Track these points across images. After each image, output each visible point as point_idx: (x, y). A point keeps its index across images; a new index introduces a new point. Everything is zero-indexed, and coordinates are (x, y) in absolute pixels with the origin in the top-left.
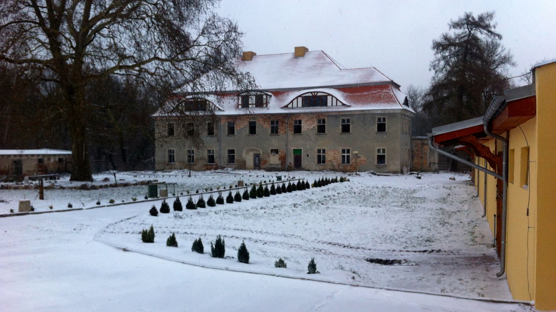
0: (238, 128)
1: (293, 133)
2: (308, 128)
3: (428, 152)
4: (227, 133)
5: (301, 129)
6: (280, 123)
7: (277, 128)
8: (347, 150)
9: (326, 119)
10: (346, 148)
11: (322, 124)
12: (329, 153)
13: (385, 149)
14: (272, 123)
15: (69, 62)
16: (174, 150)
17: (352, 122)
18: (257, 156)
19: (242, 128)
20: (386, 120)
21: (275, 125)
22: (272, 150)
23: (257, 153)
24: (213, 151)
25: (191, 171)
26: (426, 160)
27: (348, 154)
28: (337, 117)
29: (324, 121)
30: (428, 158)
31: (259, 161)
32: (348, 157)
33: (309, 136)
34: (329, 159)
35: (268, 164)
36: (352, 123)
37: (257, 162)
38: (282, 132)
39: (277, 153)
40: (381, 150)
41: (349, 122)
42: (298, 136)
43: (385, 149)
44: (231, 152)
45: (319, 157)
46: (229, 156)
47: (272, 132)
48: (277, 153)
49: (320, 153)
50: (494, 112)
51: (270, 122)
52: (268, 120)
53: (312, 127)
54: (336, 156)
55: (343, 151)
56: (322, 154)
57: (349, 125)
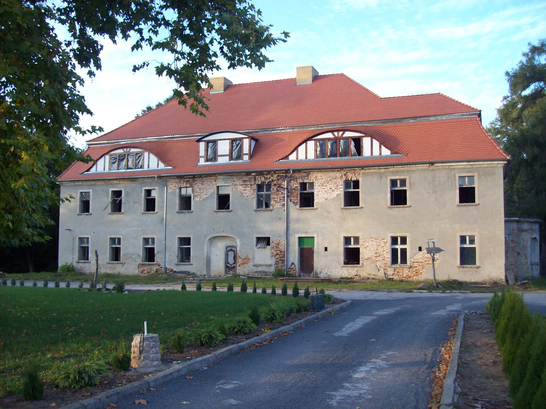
0: (197, 199)
1: (298, 206)
2: (326, 196)
3: (529, 243)
4: (177, 208)
5: (313, 200)
6: (274, 188)
7: (268, 197)
8: (470, 237)
9: (361, 180)
10: (399, 234)
11: (352, 190)
12: (367, 244)
13: (474, 237)
14: (260, 188)
15: (65, 102)
16: (88, 238)
17: (410, 184)
18: (231, 250)
19: (204, 199)
20: (476, 179)
21: (265, 192)
22: (259, 240)
23: (229, 243)
24: (153, 239)
25: (432, 278)
26: (526, 258)
27: (403, 247)
28: (381, 178)
29: (356, 184)
30: (529, 256)
31: (235, 258)
32: (404, 251)
33: (329, 212)
34: (366, 257)
35: (251, 264)
36: (410, 188)
37: (231, 261)
38: (278, 205)
39: (268, 244)
40: (399, 239)
41: (405, 185)
42: (307, 213)
43: (474, 237)
44: (186, 241)
45: (394, 252)
46: (181, 250)
47: (259, 204)
48: (268, 244)
49: (397, 244)
50: (235, 179)
51: (255, 187)
52: (253, 183)
53: (334, 194)
54: (380, 250)
55: (394, 240)
56: (399, 247)
57: (405, 191)
